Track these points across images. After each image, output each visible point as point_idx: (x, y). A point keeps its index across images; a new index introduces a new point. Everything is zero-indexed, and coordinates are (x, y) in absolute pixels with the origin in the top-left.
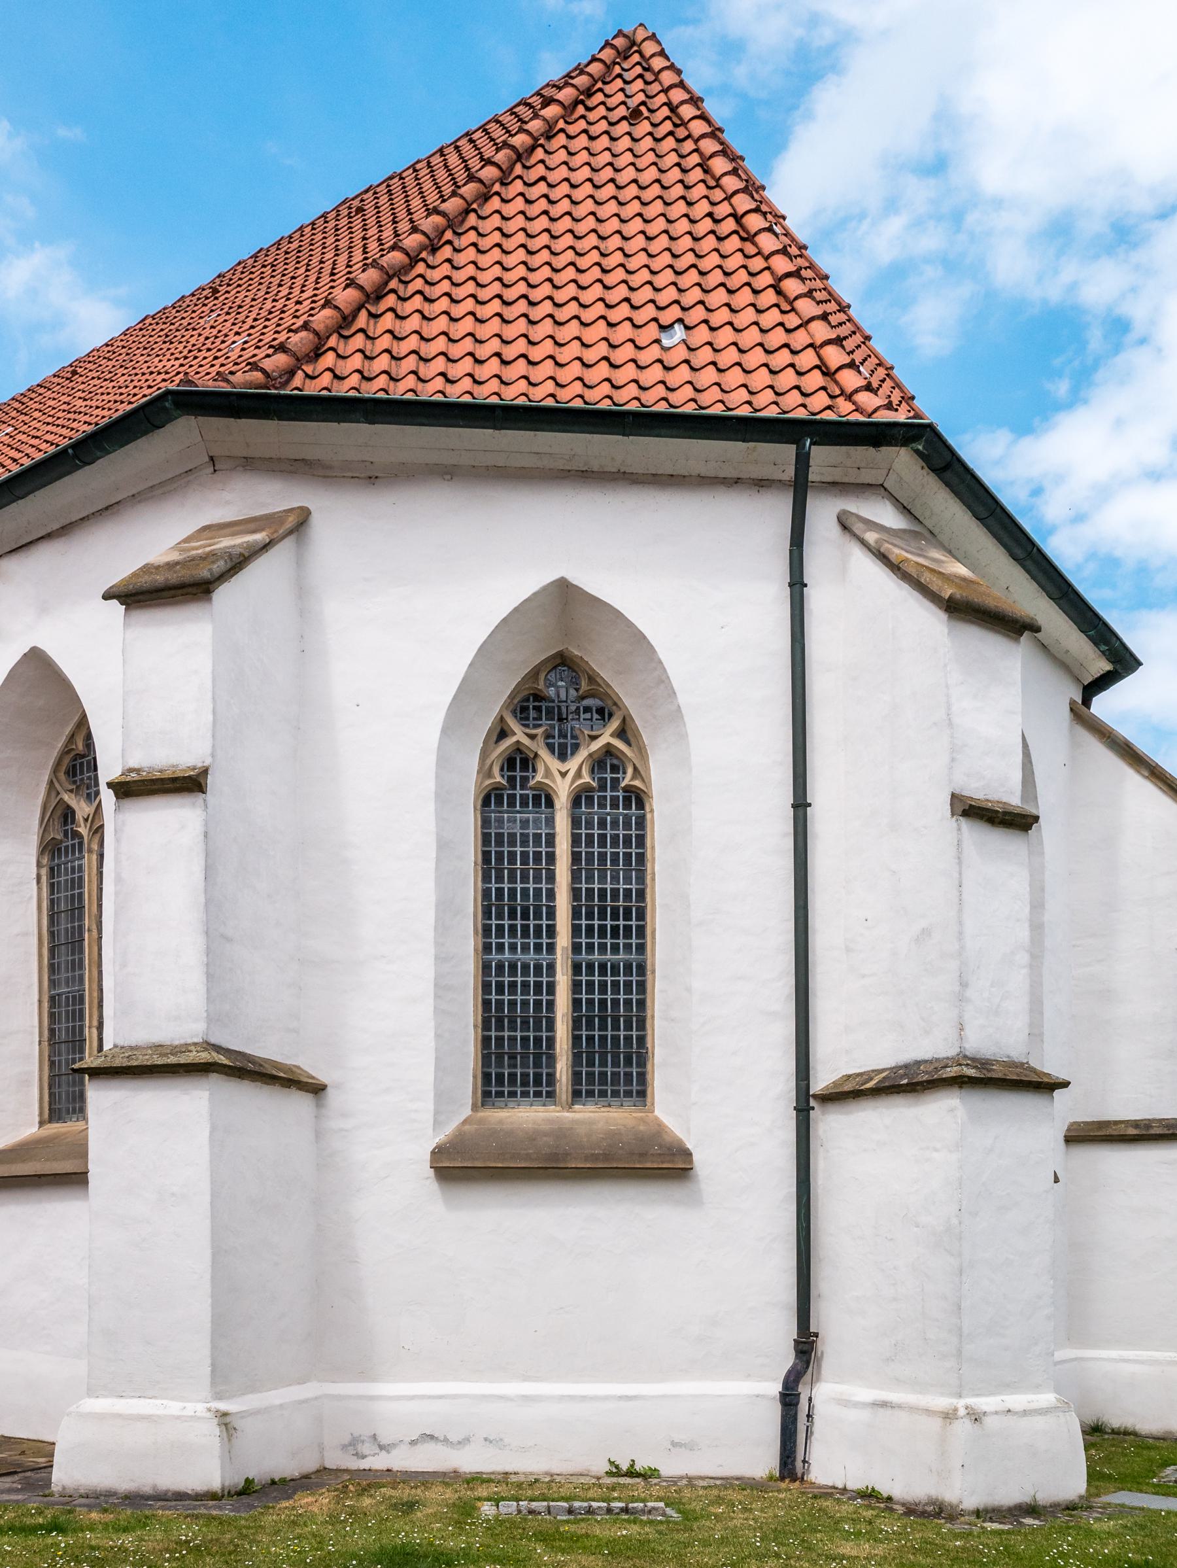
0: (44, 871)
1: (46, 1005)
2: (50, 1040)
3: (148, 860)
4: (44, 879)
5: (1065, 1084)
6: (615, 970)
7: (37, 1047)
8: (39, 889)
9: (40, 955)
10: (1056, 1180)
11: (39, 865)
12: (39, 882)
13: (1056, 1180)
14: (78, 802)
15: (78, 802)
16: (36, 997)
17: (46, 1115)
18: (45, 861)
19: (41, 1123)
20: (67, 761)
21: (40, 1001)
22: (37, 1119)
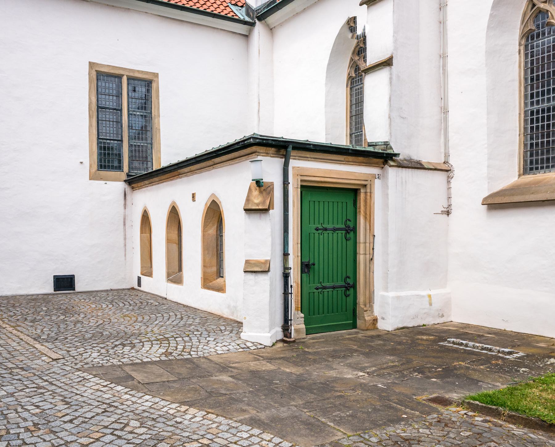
0: (522, 48)
1: (523, 116)
2: (524, 133)
3: (375, 86)
4: (522, 51)
5: (399, 154)
6: (543, 100)
7: (518, 137)
8: (520, 57)
9: (520, 91)
10: (193, 196)
11: (520, 45)
12: (519, 53)
13: (193, 196)
14: (551, 6)
15: (551, 6)
16: (518, 112)
17: (522, 172)
18: (523, 42)
19: (520, 175)
20: (357, 49)
21: (520, 114)
22: (517, 174)
